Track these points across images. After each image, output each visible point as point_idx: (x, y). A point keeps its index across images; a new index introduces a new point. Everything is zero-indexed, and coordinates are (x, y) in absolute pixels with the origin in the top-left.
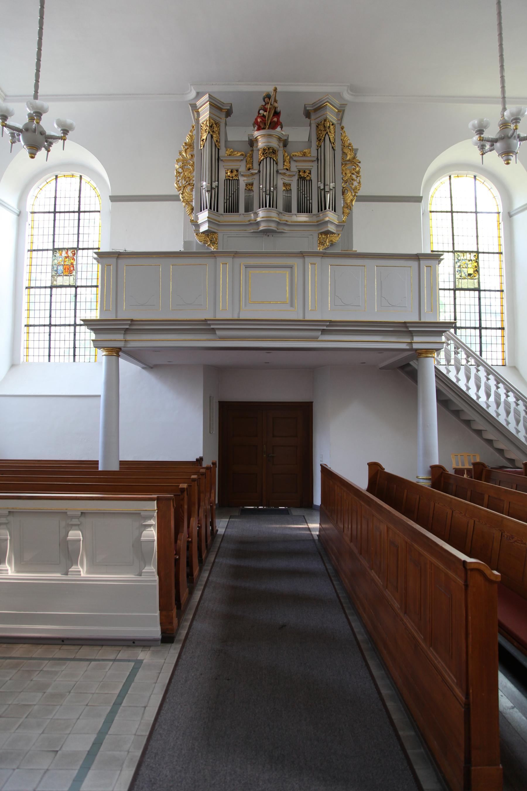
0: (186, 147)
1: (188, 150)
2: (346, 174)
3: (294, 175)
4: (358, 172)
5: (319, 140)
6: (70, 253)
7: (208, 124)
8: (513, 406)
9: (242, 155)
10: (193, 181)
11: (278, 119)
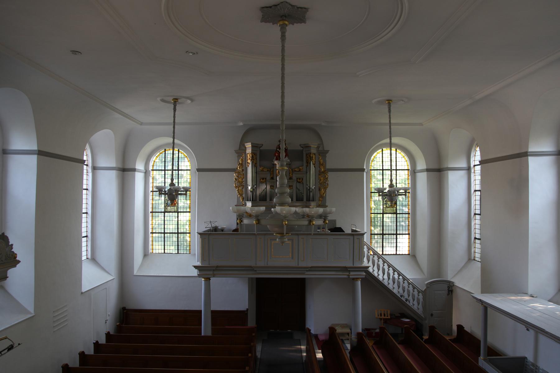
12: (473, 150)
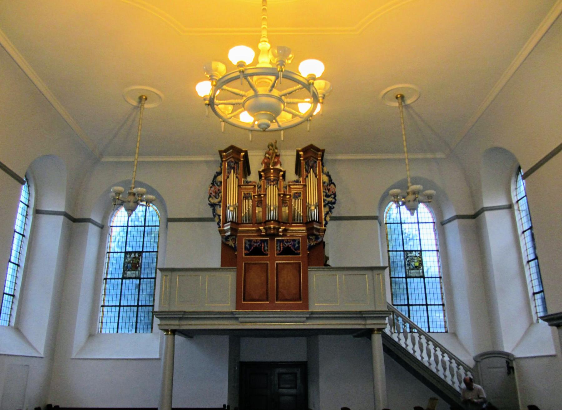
6: (137, 255)
8: (448, 364)
12: (513, 187)
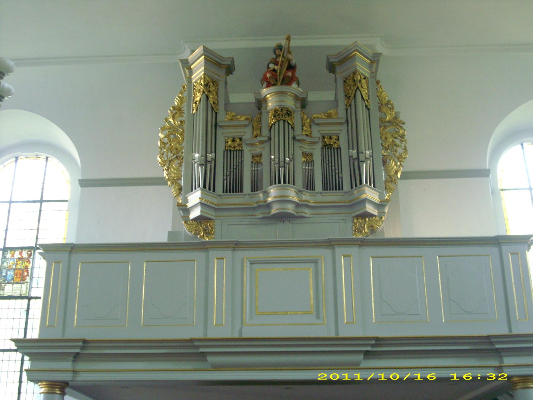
0: (174, 112)
1: (177, 115)
2: (386, 138)
3: (317, 142)
4: (402, 136)
5: (348, 97)
6: (25, 254)
7: (202, 83)
9: (247, 119)
10: (182, 153)
11: (293, 74)
